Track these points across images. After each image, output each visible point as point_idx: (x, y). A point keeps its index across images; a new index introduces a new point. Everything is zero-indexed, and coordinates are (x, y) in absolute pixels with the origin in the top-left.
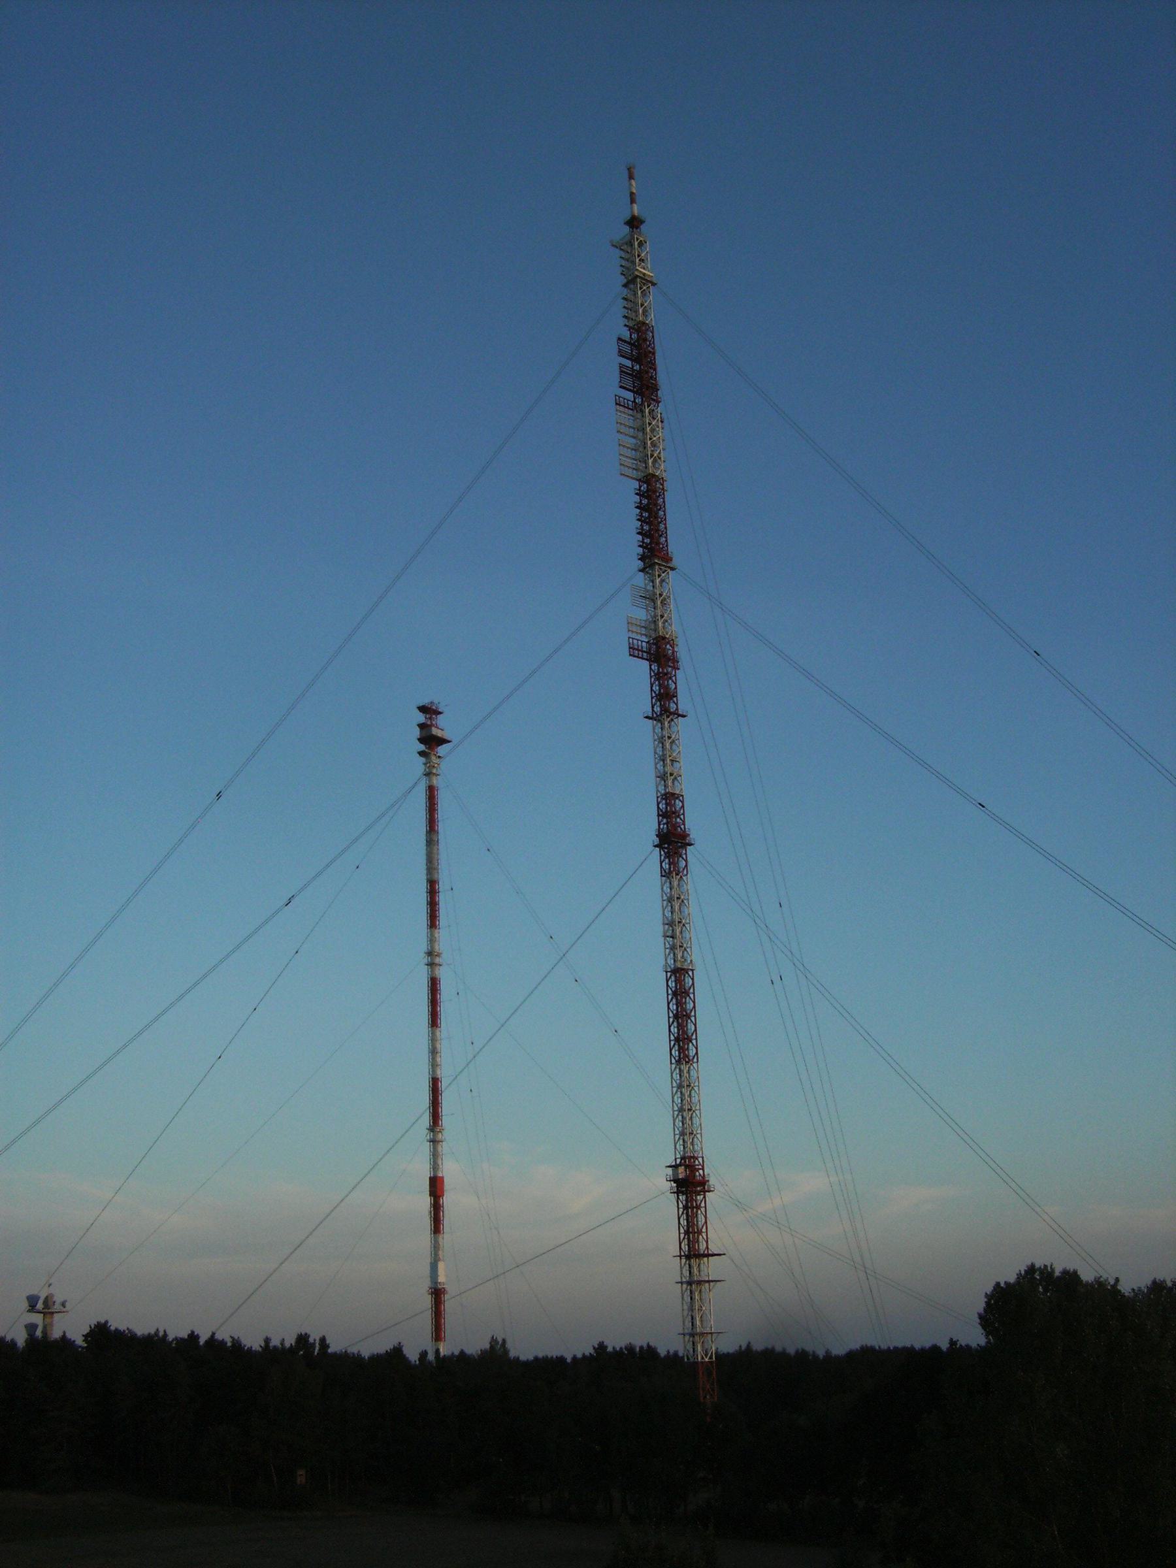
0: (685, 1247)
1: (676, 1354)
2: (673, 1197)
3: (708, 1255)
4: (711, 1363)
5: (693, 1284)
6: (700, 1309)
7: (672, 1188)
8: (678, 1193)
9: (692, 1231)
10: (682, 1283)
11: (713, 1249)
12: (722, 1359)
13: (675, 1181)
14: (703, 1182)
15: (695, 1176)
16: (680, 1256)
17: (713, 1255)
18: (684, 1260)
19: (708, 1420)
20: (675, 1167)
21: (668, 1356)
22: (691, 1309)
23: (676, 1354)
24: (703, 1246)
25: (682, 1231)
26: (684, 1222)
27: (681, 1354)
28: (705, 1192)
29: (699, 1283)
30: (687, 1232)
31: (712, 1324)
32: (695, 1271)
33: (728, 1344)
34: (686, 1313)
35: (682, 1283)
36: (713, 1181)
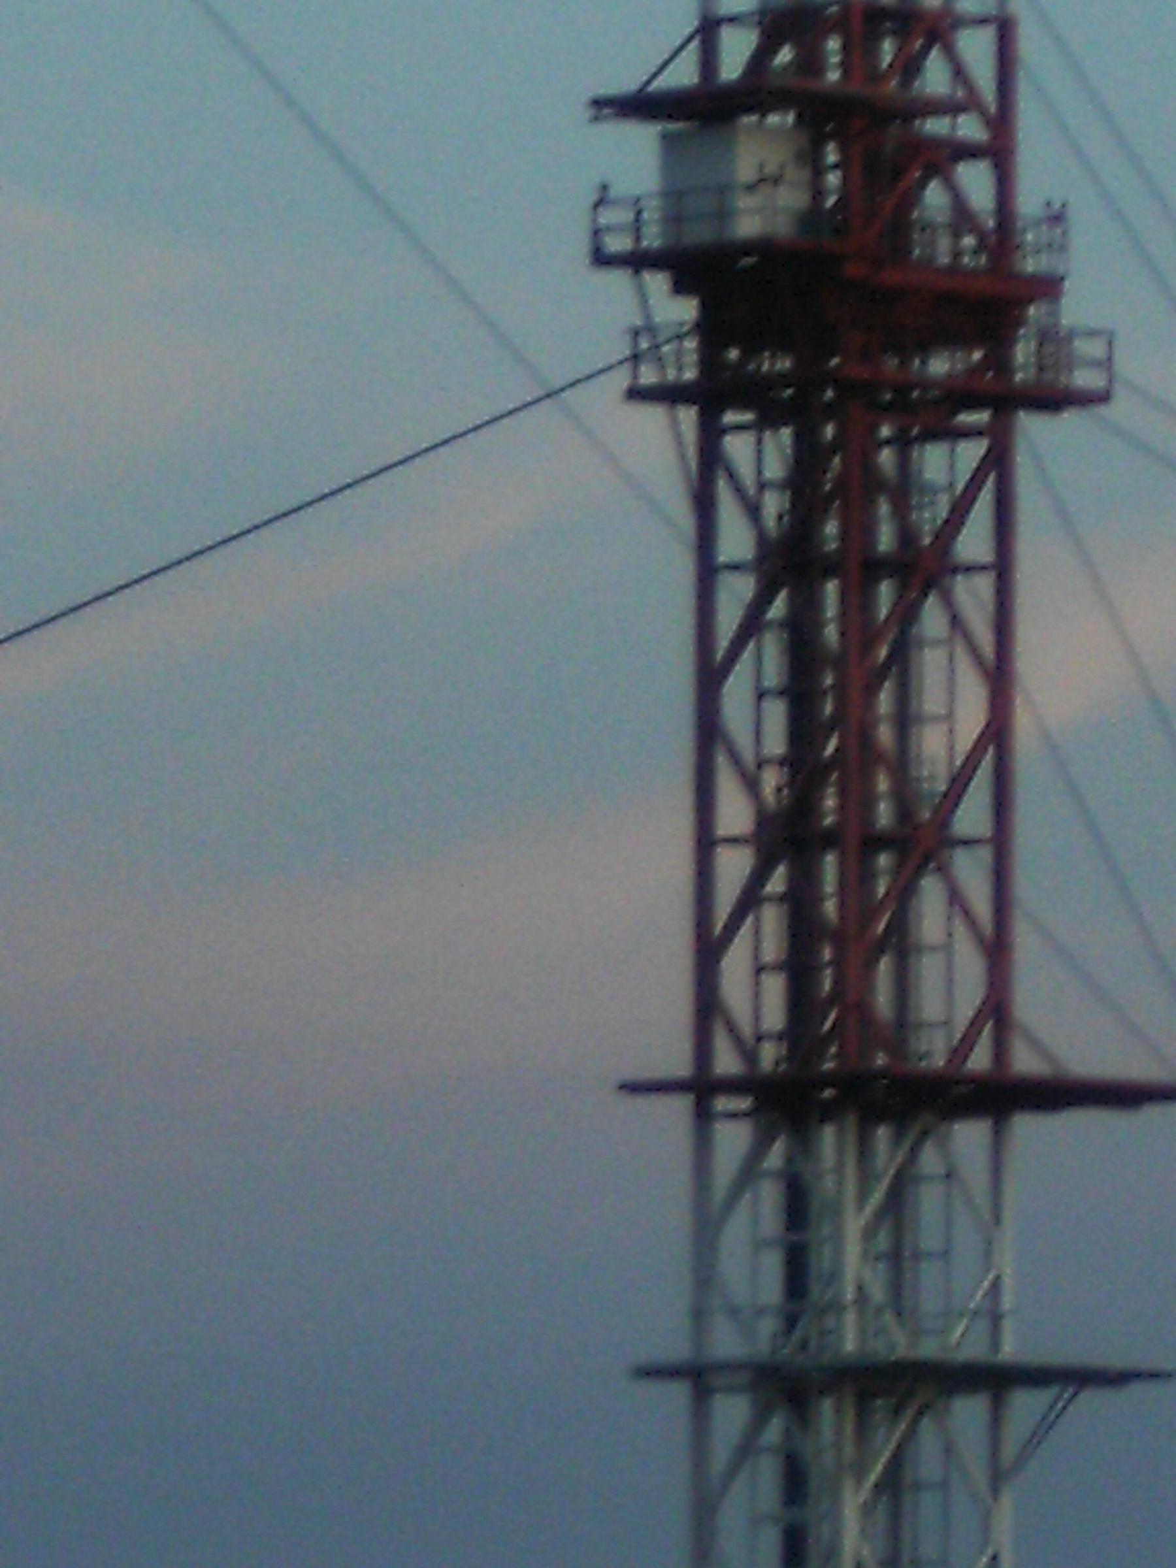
0: (756, 996)
2: (657, 442)
3: (1004, 1097)
7: (644, 342)
8: (711, 395)
9: (839, 824)
10: (699, 1377)
11: (1060, 1030)
13: (688, 267)
14: (994, 301)
15: (900, 227)
16: (702, 1088)
17: (1058, 1094)
18: (732, 1139)
20: (697, 112)
24: (944, 990)
25: (734, 814)
26: (756, 719)
28: (1006, 401)
29: (903, 1385)
30: (788, 836)
32: (851, 1255)
35: (699, 1377)
36: (1096, 294)
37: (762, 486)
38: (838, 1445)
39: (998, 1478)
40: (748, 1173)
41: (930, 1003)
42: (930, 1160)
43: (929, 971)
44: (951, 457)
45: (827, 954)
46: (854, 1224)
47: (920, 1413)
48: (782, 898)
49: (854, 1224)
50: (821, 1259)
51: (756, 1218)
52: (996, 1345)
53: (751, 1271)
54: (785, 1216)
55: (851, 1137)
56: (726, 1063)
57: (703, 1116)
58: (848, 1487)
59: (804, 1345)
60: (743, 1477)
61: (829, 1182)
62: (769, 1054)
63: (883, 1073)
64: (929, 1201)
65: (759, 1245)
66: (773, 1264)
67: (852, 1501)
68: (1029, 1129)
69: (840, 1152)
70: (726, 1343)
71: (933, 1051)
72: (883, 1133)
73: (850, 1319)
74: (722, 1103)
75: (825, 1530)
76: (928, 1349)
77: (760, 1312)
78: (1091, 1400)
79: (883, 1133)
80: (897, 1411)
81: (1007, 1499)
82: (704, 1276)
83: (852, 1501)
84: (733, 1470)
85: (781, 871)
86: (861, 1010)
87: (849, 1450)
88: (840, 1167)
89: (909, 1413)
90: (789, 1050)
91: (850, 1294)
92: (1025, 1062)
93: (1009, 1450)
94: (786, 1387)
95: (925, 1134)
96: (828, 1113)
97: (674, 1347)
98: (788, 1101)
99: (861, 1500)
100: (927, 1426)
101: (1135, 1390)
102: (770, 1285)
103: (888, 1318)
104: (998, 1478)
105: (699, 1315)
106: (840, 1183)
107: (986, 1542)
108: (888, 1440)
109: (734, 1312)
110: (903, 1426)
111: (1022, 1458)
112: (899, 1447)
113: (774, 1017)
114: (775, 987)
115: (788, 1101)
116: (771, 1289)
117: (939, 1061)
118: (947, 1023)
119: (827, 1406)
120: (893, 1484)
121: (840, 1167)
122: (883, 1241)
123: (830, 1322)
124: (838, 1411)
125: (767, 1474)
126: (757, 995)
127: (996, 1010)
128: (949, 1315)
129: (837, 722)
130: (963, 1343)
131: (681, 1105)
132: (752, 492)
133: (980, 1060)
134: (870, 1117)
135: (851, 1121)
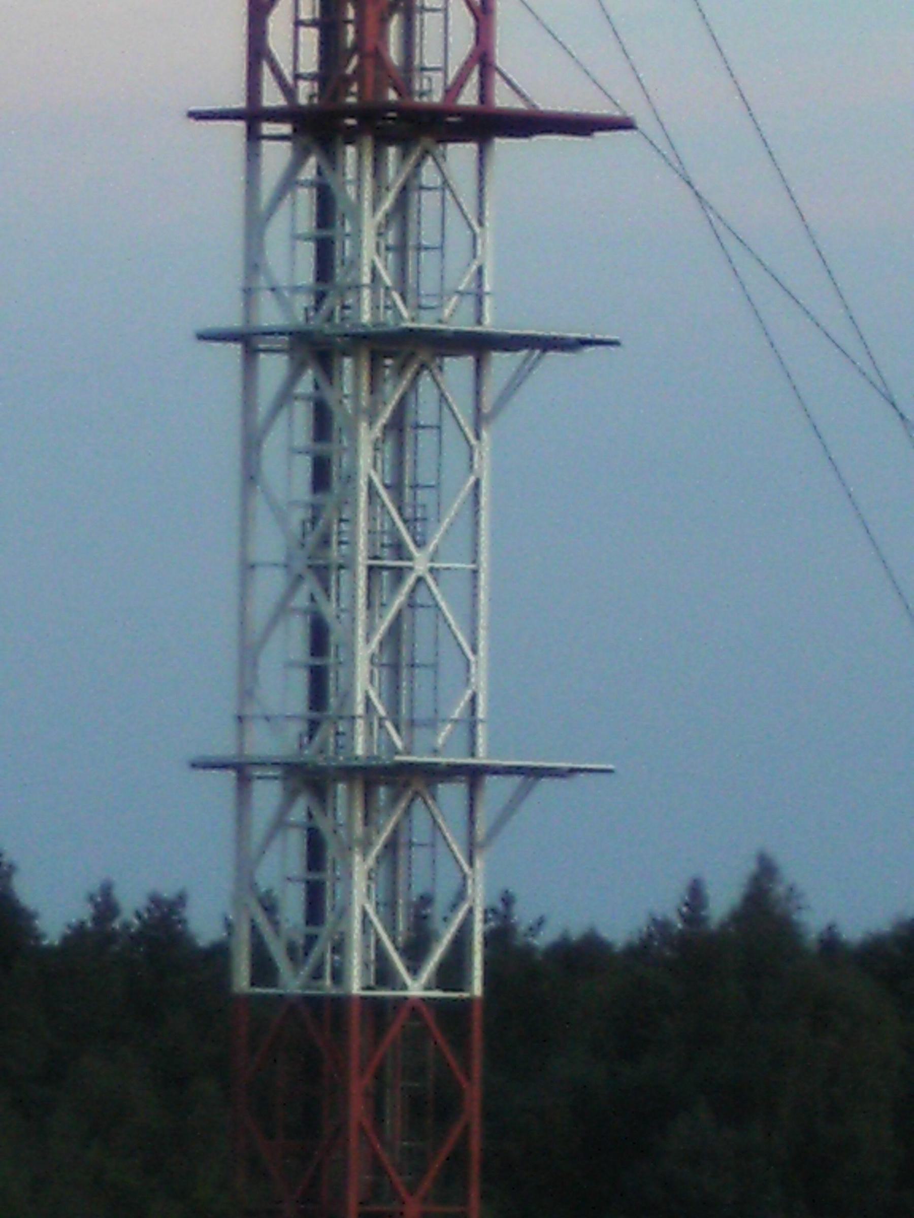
1: (165, 917)
3: (486, 126)
4: (453, 1015)
5: (350, 356)
6: (389, 570)
10: (249, 341)
11: (531, 74)
12: (542, 989)
16: (253, 116)
17: (529, 124)
18: (276, 155)
19: (656, 943)
21: (96, 938)
22: (319, 565)
23: (165, 917)
27: (204, 925)
29: (405, 349)
31: (478, 698)
32: (366, 247)
33: (598, 876)
34: (270, 585)
35: (249, 341)
37: (297, 77)
38: (356, 396)
39: (479, 419)
40: (289, 182)
41: (429, 53)
42: (429, 174)
43: (429, 26)
44: (442, 262)
45: (351, 14)
46: (370, 223)
48: (311, 184)
49: (370, 223)
51: (293, 219)
52: (479, 322)
53: (291, 260)
54: (305, 847)
55: (365, 363)
56: (272, 97)
57: (254, 137)
59: (330, 318)
60: (276, 844)
61: (351, 190)
62: (305, 92)
63: (392, 107)
64: (428, 204)
65: (294, 451)
66: (307, 252)
67: (361, 866)
68: (504, 147)
69: (357, 376)
70: (270, 315)
71: (431, 90)
72: (392, 152)
74: (267, 128)
75: (345, 460)
76: (426, 322)
77: (295, 289)
78: (553, 356)
79: (392, 152)
80: (400, 370)
81: (479, 863)
82: (254, 264)
83: (361, 866)
84: (270, 837)
85: (312, 161)
86: (378, 56)
87: (359, 829)
88: (359, 179)
90: (320, 88)
92: (503, 99)
93: (481, 829)
94: (316, 349)
95: (426, 153)
96: (351, 137)
97: (223, 746)
98: (319, 128)
99: (369, 652)
100: (426, 379)
102: (305, 271)
103: (396, 296)
104: (479, 419)
105: (248, 292)
110: (405, 383)
113: (310, 62)
114: (310, 37)
115: (319, 128)
116: (306, 274)
117: (437, 98)
118: (444, 70)
119: (341, 787)
120: (398, 426)
121: (359, 179)
122: (391, 237)
125: (301, 415)
126: (293, 263)
127: (482, 59)
128: (442, 296)
129: (358, 47)
130: (455, 317)
132: (289, 79)
133: (469, 98)
134: (382, 140)
135: (368, 143)
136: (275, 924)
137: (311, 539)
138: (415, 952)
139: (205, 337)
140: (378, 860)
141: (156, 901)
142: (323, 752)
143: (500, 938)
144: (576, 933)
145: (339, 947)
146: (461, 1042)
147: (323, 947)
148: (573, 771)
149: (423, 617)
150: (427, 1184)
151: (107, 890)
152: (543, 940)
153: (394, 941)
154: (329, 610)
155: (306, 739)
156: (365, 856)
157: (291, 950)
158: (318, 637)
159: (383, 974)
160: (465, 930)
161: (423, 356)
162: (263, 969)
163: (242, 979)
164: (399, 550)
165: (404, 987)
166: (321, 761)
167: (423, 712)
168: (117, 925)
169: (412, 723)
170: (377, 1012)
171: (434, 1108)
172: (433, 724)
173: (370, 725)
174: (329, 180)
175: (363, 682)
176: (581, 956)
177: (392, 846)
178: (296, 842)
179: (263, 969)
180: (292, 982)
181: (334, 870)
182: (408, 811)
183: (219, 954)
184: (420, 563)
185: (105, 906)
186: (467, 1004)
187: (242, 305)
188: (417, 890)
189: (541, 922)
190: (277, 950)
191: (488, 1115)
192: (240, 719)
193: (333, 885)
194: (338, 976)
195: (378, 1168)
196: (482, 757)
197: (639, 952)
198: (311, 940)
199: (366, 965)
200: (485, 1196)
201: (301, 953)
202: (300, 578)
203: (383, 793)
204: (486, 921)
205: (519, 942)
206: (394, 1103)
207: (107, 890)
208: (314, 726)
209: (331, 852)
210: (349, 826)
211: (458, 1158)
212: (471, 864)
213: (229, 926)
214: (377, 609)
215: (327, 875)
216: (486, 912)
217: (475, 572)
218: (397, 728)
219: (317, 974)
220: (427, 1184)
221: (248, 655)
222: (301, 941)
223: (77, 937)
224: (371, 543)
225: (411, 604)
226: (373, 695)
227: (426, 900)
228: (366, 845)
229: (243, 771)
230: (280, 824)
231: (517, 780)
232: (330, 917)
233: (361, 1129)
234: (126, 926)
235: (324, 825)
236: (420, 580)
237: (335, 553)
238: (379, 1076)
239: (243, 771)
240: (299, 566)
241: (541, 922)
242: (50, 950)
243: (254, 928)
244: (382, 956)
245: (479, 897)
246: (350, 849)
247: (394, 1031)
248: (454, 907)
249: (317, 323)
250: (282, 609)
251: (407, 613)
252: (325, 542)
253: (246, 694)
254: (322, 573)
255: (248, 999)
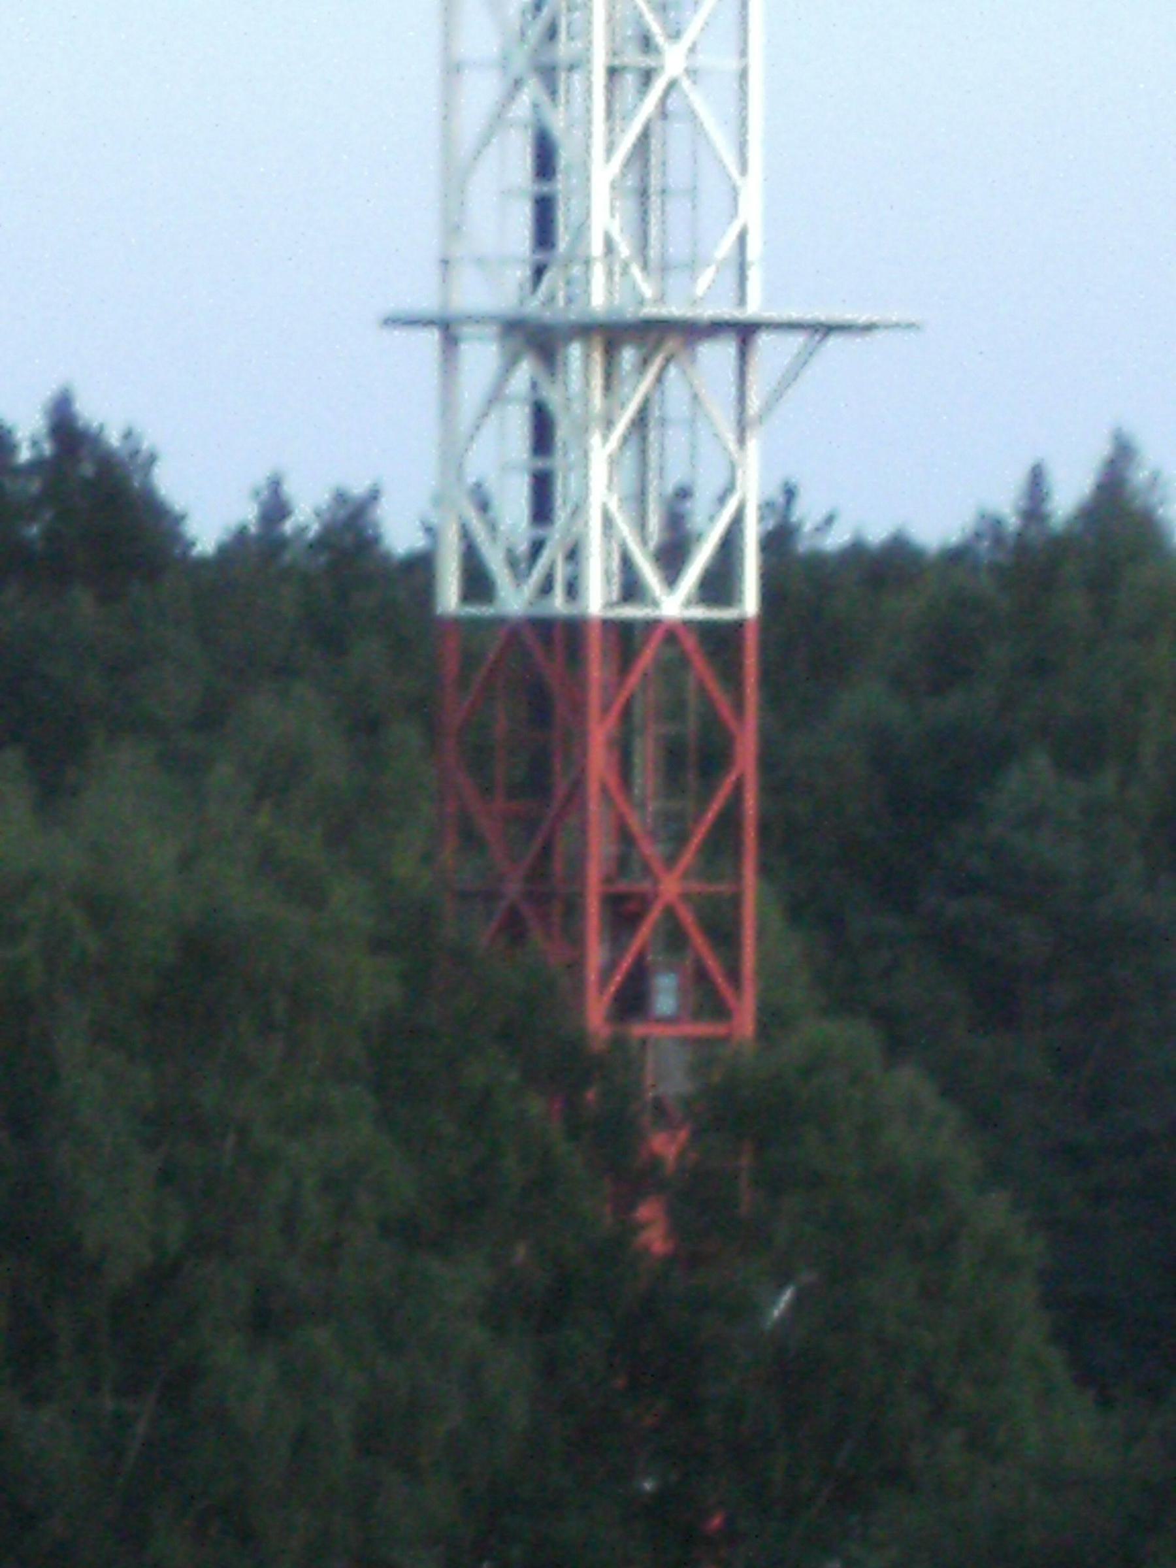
4: (721, 640)
6: (635, 70)
12: (832, 609)
21: (260, 549)
27: (400, 535)
31: (747, 229)
34: (481, 91)
47: (668, 360)
50: (563, 491)
55: (597, 356)
58: (595, 439)
59: (551, 298)
60: (492, 151)
65: (507, 193)
67: (601, 450)
73: (598, 273)
80: (645, 362)
81: (753, 444)
83: (601, 450)
89: (658, 361)
91: (597, 248)
93: (754, 404)
94: (536, 340)
97: (423, 298)
100: (673, 371)
101: (878, 336)
103: (635, 270)
106: (587, 383)
107: (734, 212)
108: (635, 389)
109: (480, 261)
111: (768, 407)
112: (645, 136)
119: (575, 351)
123: (576, 270)
124: (587, 357)
131: (431, 338)
136: (493, 527)
137: (535, 31)
138: (672, 558)
139: (394, 321)
140: (625, 440)
141: (340, 497)
142: (552, 303)
143: (778, 541)
144: (877, 534)
145: (573, 554)
146: (731, 674)
147: (553, 553)
148: (869, 328)
149: (678, 129)
150: (688, 857)
151: (275, 485)
152: (836, 540)
153: (644, 541)
154: (558, 123)
155: (529, 17)
156: (605, 438)
157: (512, 562)
158: (545, 159)
159: (632, 589)
160: (737, 521)
161: (671, 344)
162: (477, 583)
163: (449, 596)
164: (646, 43)
165: (655, 604)
166: (547, 315)
167: (678, 250)
168: (288, 527)
169: (665, 268)
170: (625, 637)
171: (697, 759)
172: (693, 266)
173: (610, 274)
174: (544, 393)
175: (599, 207)
176: (888, 567)
177: (641, 421)
178: (517, 424)
179: (477, 583)
180: (513, 599)
181: (566, 454)
182: (659, 379)
183: (421, 566)
184: (673, 60)
185: (275, 508)
186: (738, 626)
187: (438, 146)
188: (675, 478)
189: (829, 520)
190: (495, 562)
191: (768, 762)
192: (445, 262)
193: (565, 478)
194: (573, 589)
195: (625, 836)
196: (754, 309)
197: (955, 557)
198: (537, 547)
199: (607, 573)
200: (764, 870)
201: (523, 566)
202: (518, 84)
203: (628, 356)
204: (761, 519)
205: (803, 546)
206: (646, 753)
207: (275, 485)
208: (539, 272)
209: (562, 432)
210: (587, 402)
211: (730, 820)
212: (741, 441)
213: (429, 530)
214: (618, 122)
215: (560, 185)
216: (760, 507)
217: (743, 75)
218: (645, 267)
219: (546, 588)
220: (688, 857)
221: (454, 181)
222: (523, 548)
223: (239, 545)
224: (612, 34)
225: (663, 112)
226: (613, 506)
227: (684, 493)
228: (609, 424)
229: (449, 330)
230: (496, 397)
231: (797, 341)
232: (561, 515)
233: (604, 790)
234: (303, 529)
235: (553, 398)
236: (672, 85)
237: (564, 49)
238: (626, 713)
239: (449, 330)
240: (520, 61)
241: (829, 520)
242: (203, 563)
243: (466, 535)
244: (627, 562)
245: (753, 490)
246: (586, 430)
247: (647, 658)
248: (722, 500)
249: (533, 307)
250: (498, 119)
251: (657, 127)
252: (552, 33)
253: (453, 228)
254: (548, 74)
255: (456, 623)
